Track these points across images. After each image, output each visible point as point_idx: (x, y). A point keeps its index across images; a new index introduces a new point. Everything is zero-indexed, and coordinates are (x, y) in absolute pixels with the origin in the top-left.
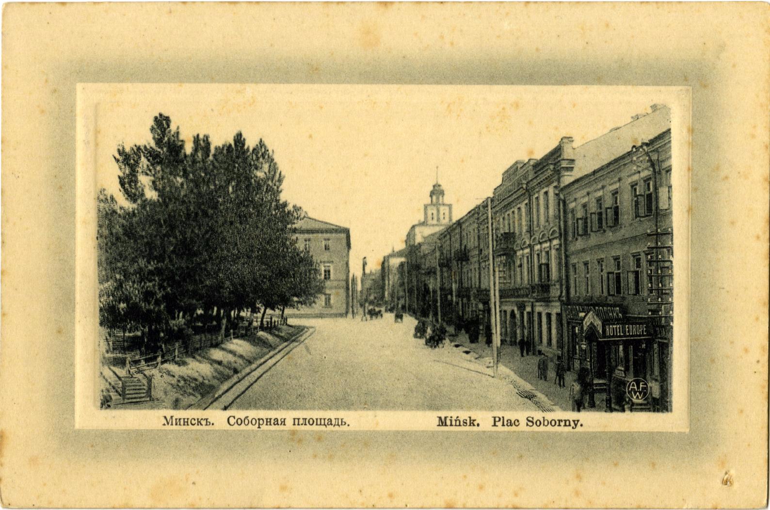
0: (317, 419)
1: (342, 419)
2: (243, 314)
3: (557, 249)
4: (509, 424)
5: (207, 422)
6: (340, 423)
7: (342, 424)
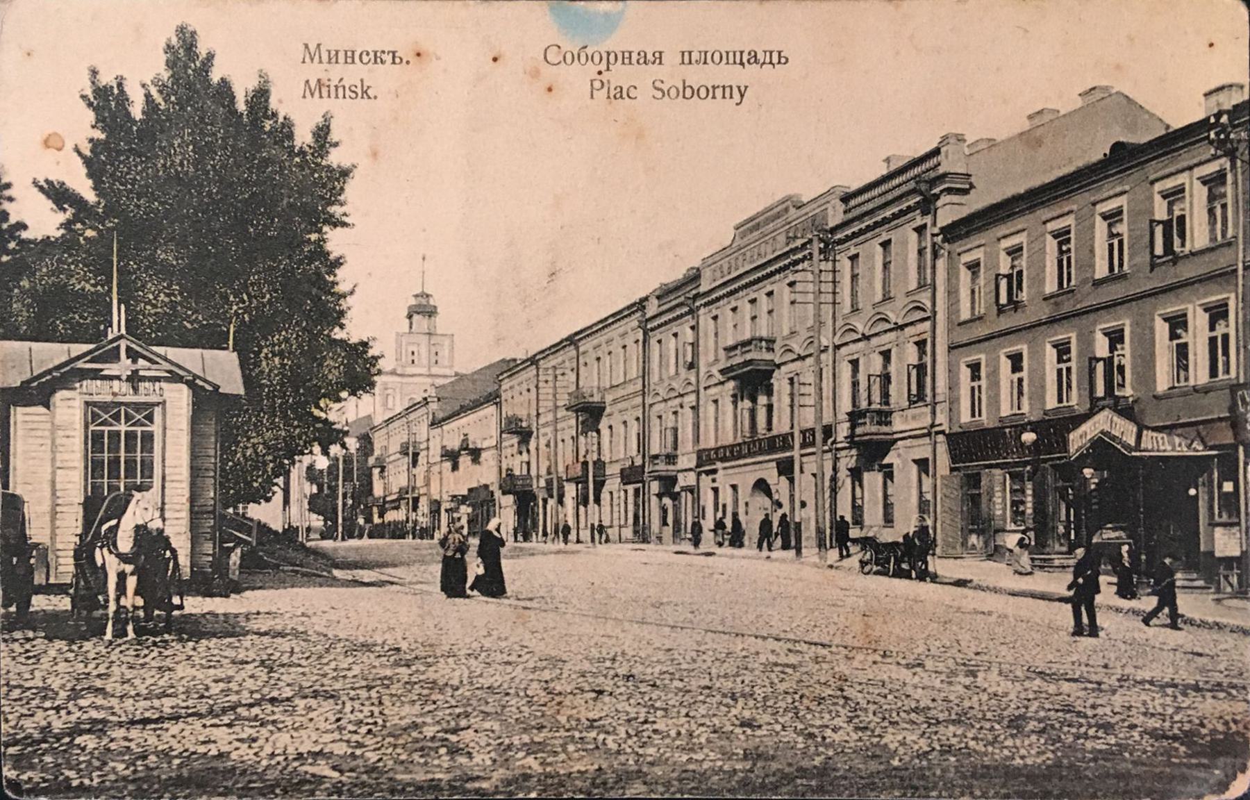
0: (727, 53)
1: (780, 53)
2: (267, 128)
3: (693, 408)
4: (642, 61)
5: (394, 57)
6: (775, 60)
7: (779, 62)
